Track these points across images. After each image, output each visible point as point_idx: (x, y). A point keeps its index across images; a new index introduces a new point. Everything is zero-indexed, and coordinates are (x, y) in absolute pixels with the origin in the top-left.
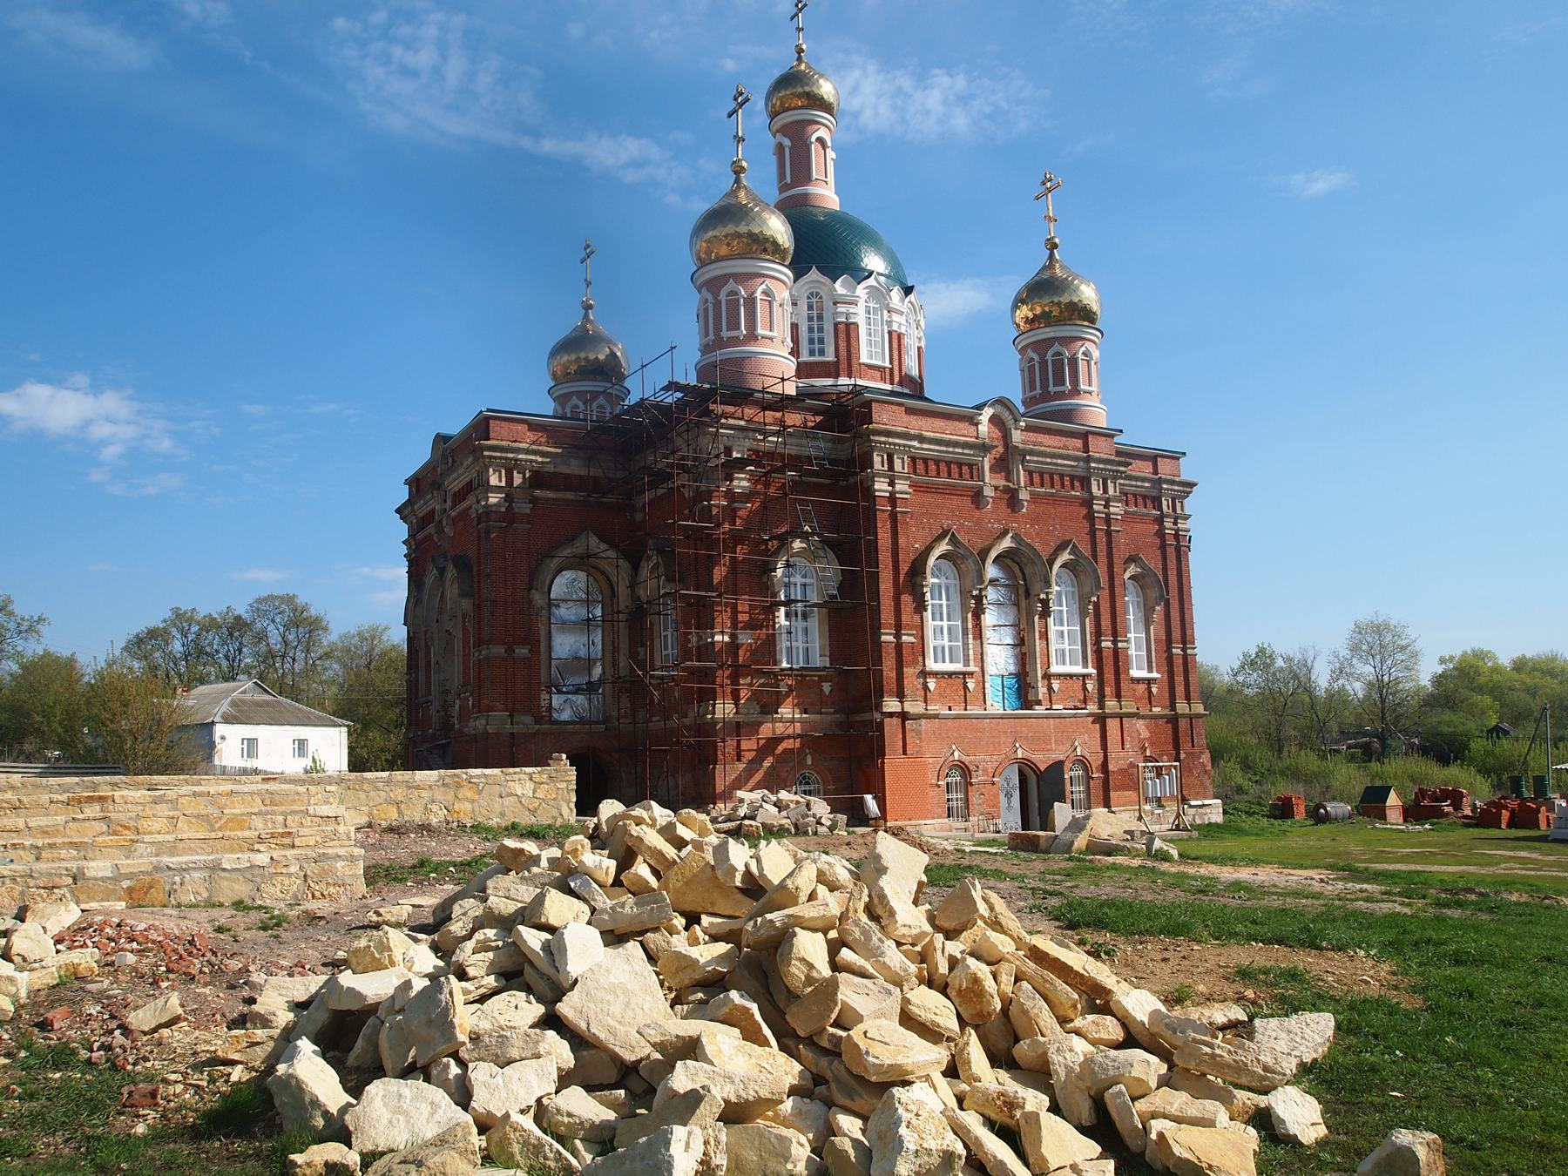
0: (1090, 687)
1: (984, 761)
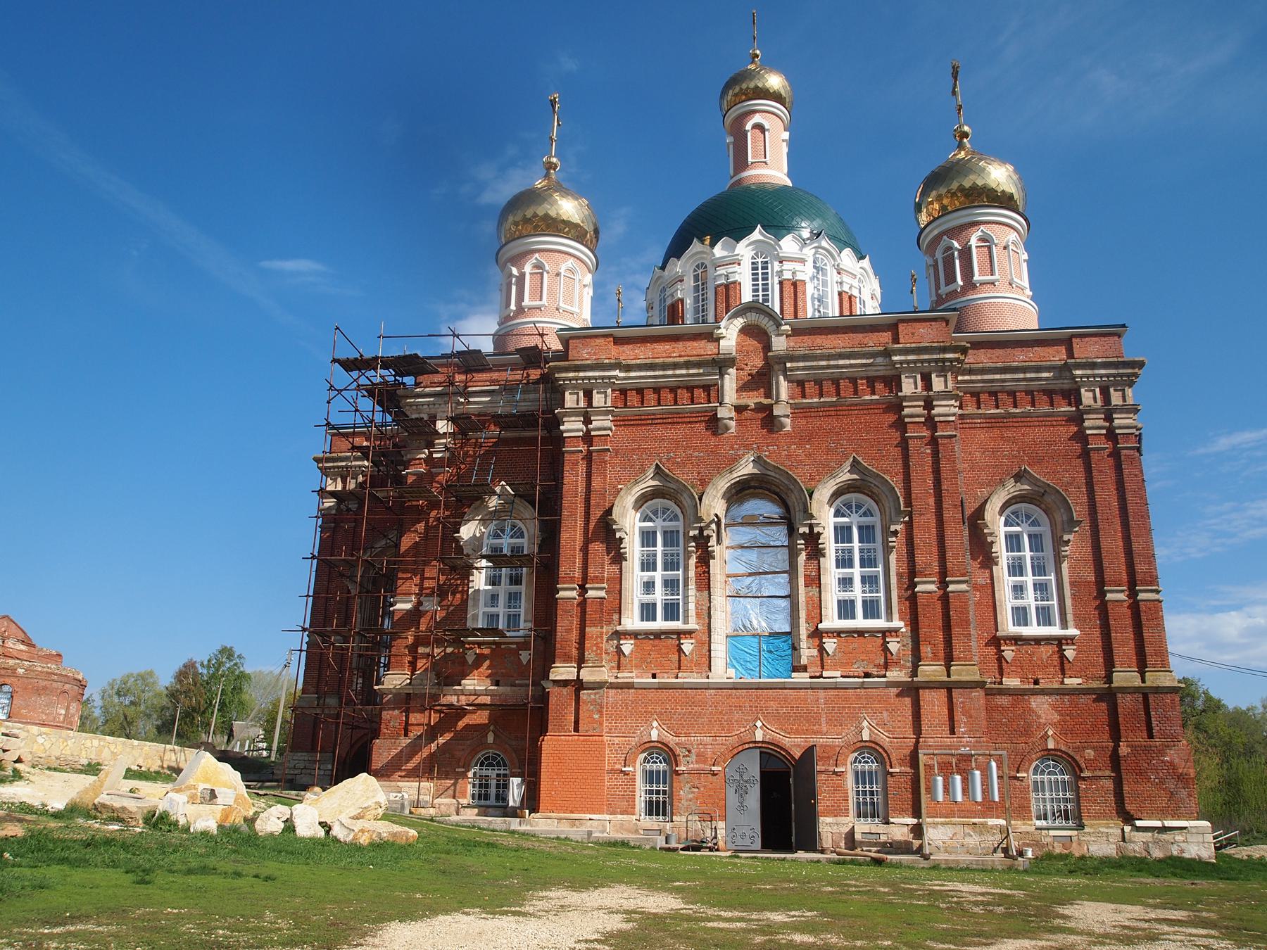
0: (893, 646)
1: (700, 744)
